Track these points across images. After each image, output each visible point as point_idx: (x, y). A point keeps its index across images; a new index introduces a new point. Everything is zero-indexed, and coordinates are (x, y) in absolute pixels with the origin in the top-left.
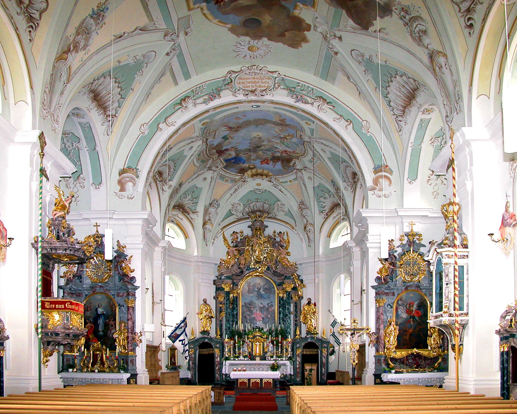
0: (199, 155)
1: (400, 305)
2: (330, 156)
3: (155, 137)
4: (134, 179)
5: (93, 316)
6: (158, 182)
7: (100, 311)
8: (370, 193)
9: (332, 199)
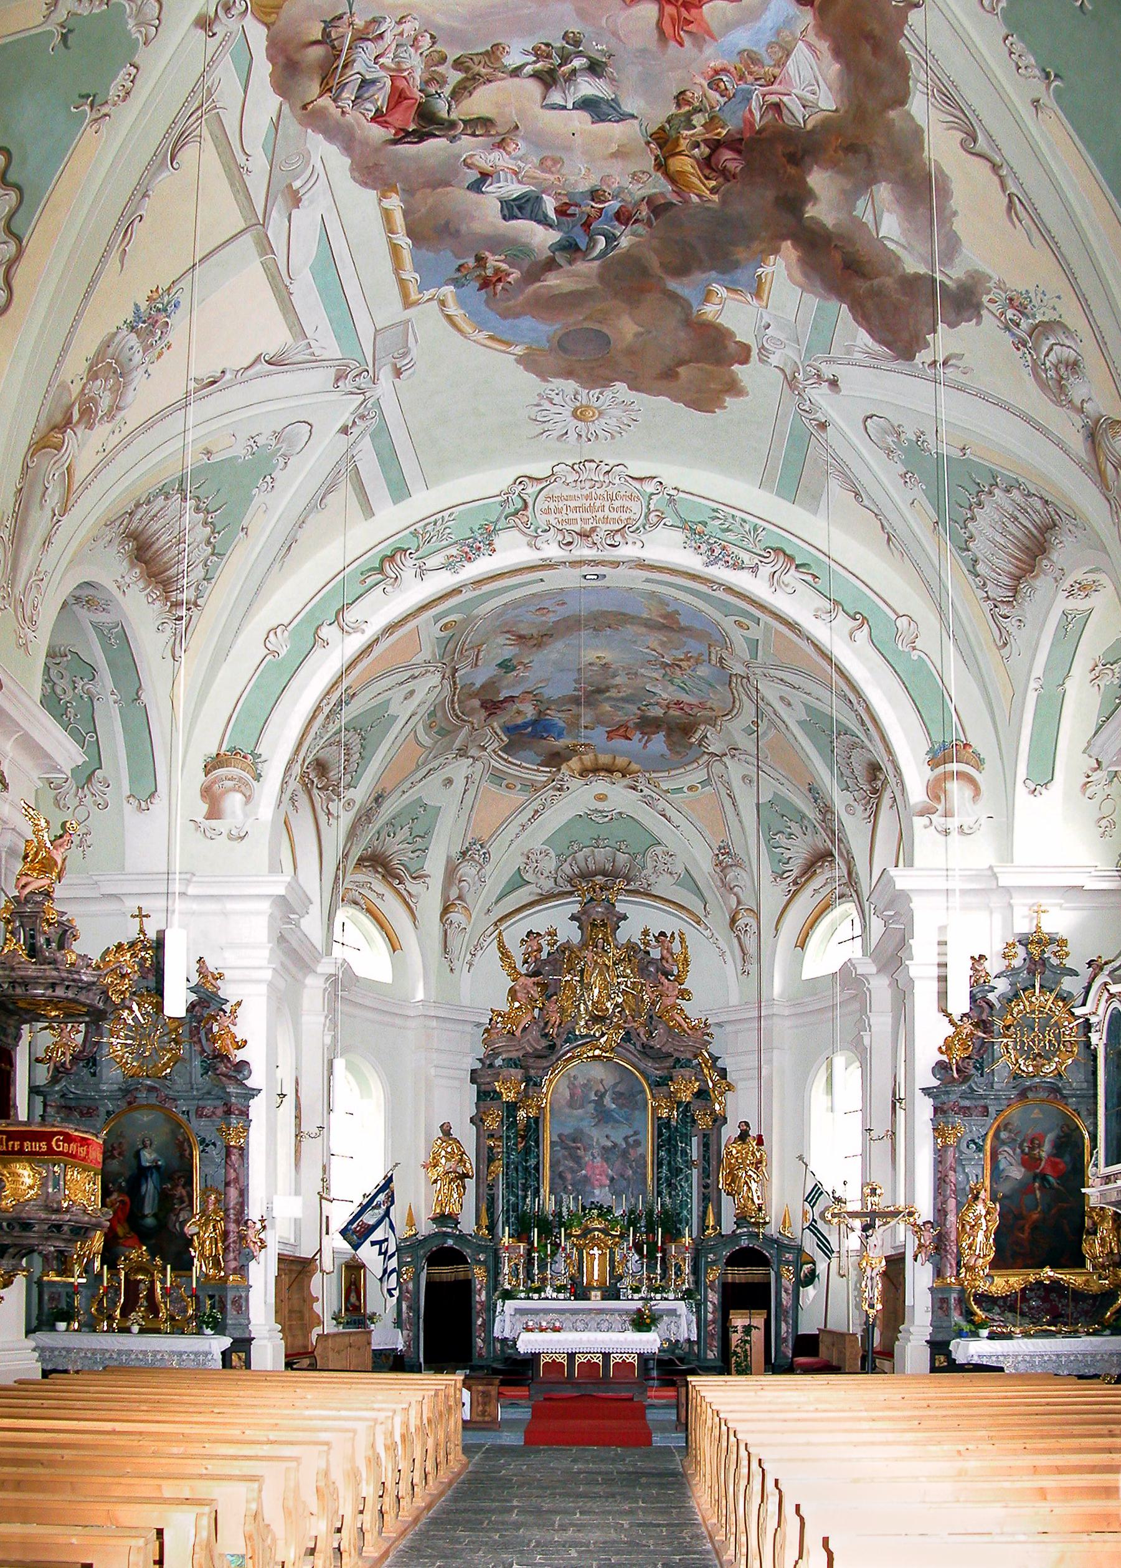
0: (432, 714)
1: (1003, 1143)
5: (128, 1174)
6: (315, 791)
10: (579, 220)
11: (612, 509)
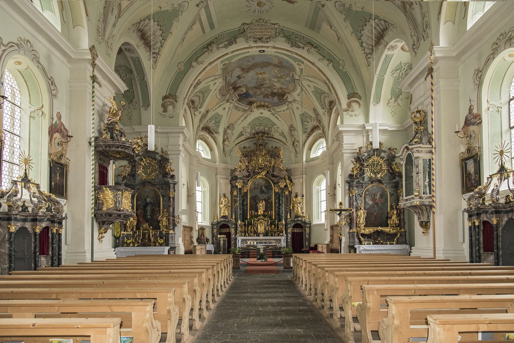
0: (220, 90)
1: (367, 195)
4: (173, 103)
7: (148, 200)
9: (312, 123)
11: (267, 32)
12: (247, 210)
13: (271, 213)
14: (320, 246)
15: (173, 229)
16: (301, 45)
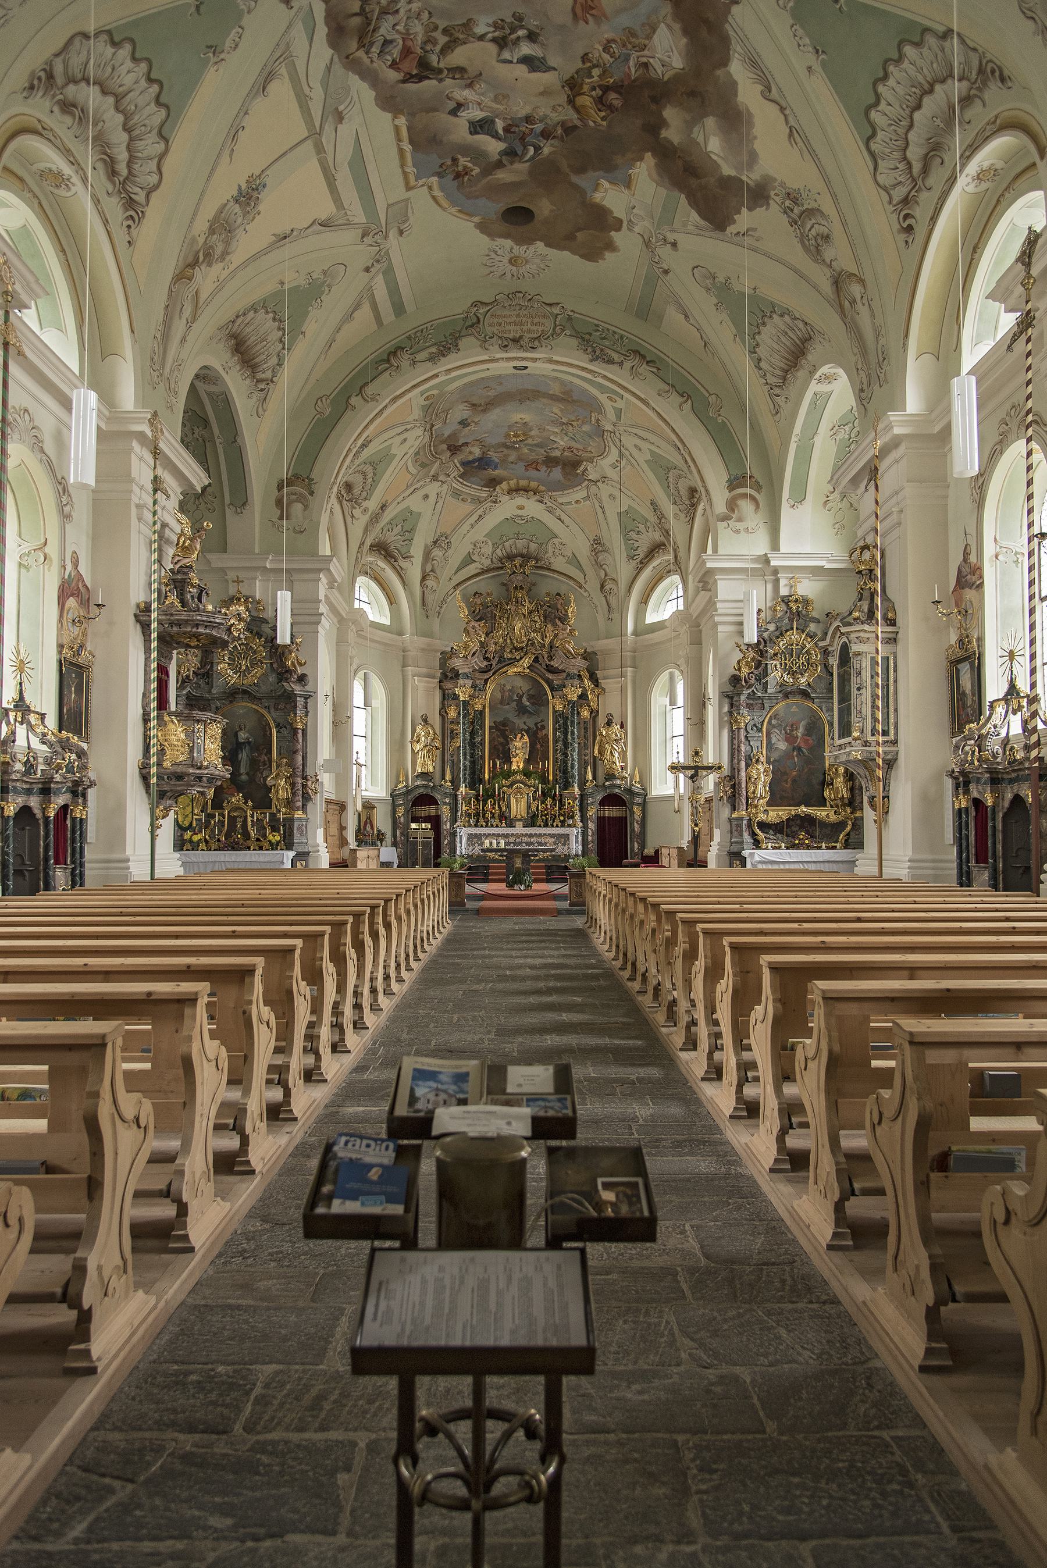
0: (417, 454)
1: (774, 727)
2: (649, 457)
3: (342, 421)
6: (345, 502)
7: (243, 736)
8: (721, 525)
9: (650, 534)
10: (518, 136)
11: (533, 324)
12: (483, 757)
13: (544, 765)
14: (664, 852)
15: (304, 808)
16: (616, 356)
